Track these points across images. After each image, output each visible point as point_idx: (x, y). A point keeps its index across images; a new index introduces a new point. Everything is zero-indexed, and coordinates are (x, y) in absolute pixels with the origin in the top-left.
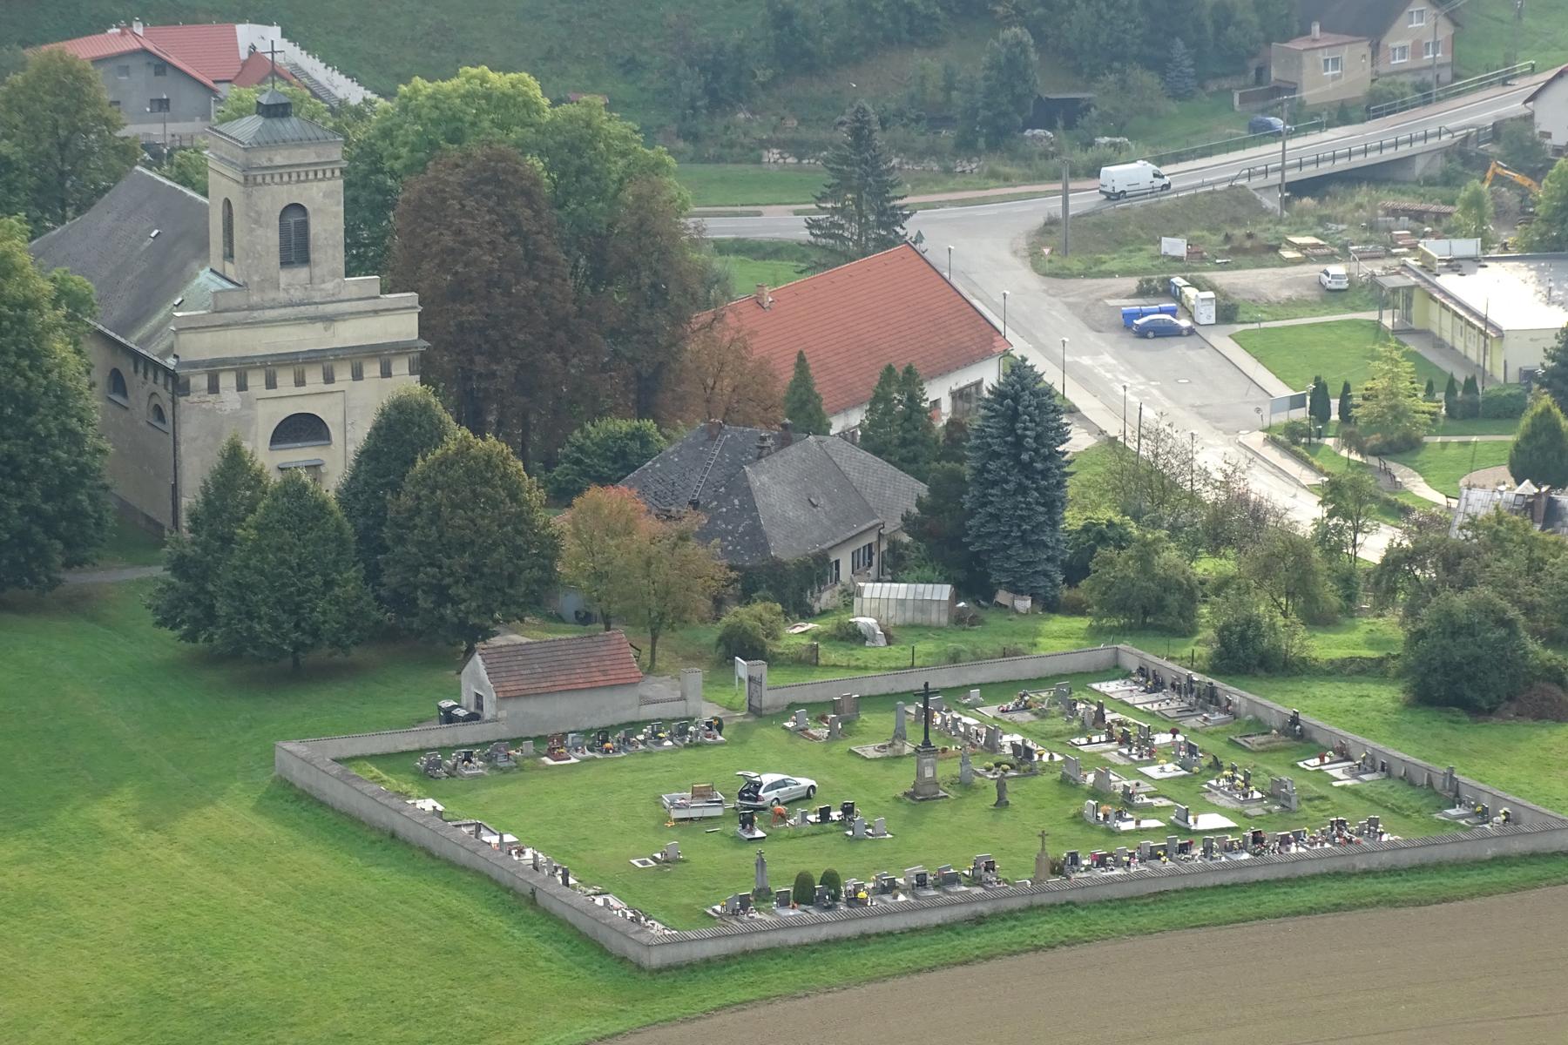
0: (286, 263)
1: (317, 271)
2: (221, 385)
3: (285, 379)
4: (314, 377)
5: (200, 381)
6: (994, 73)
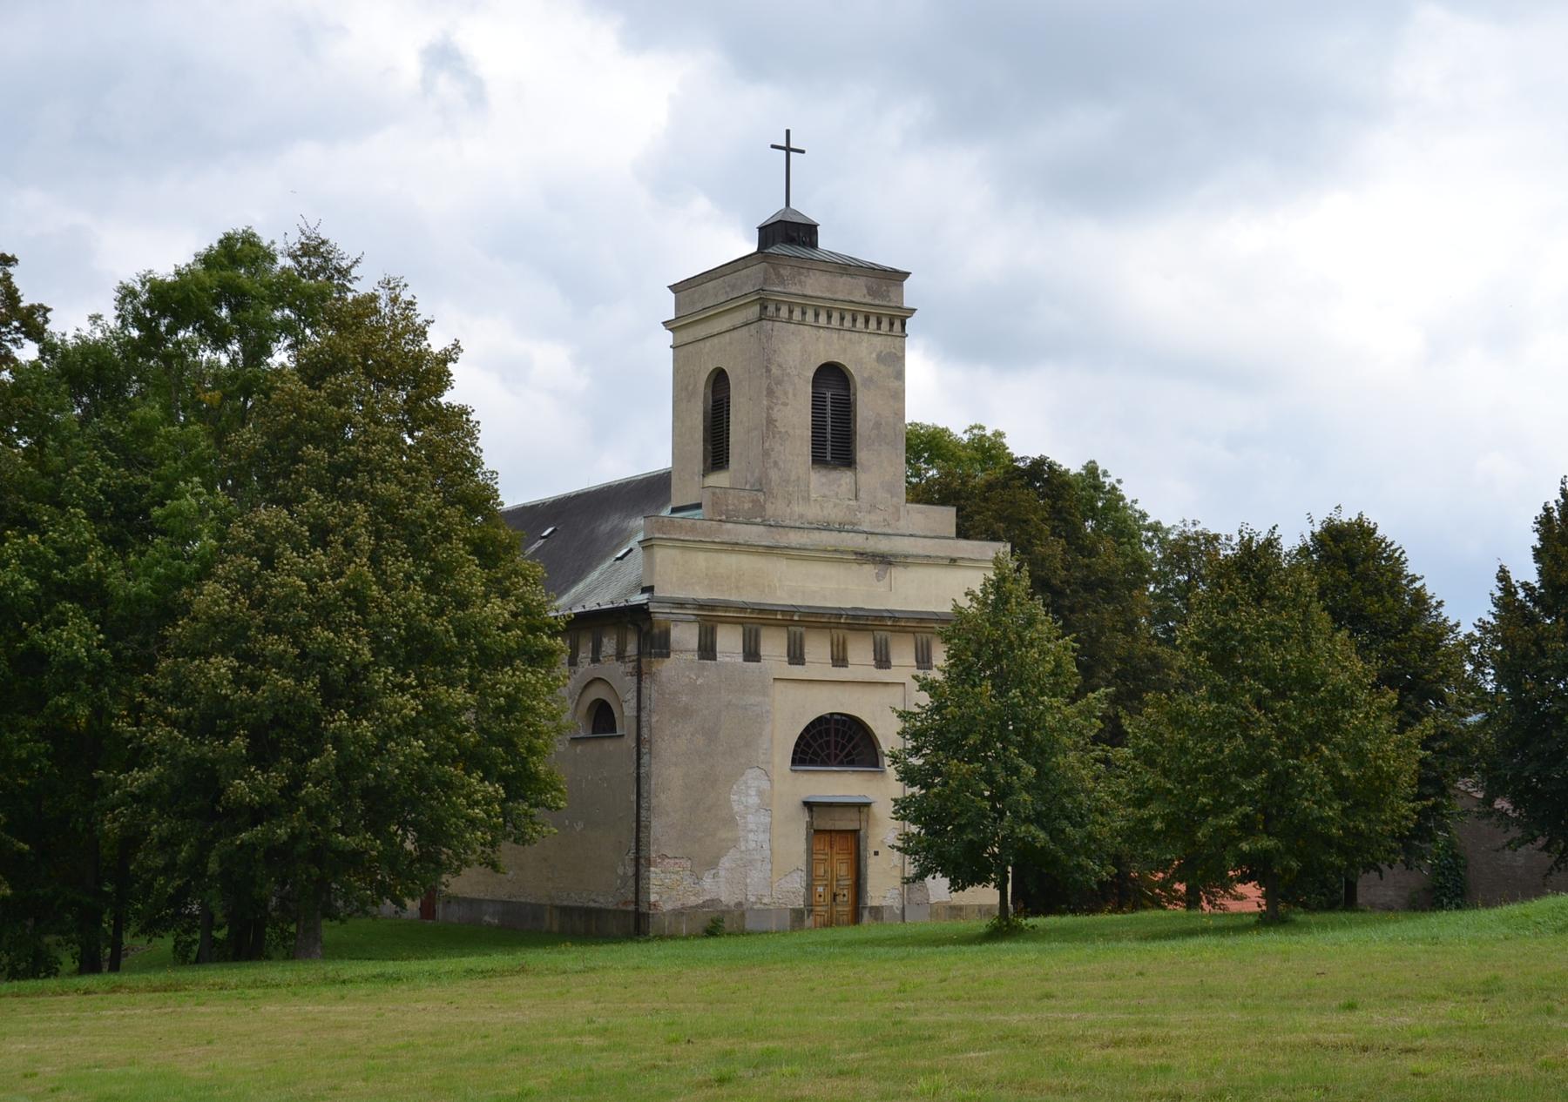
0: (818, 459)
1: (863, 477)
2: (719, 647)
3: (818, 649)
4: (860, 653)
5: (685, 636)
6: (454, 356)
